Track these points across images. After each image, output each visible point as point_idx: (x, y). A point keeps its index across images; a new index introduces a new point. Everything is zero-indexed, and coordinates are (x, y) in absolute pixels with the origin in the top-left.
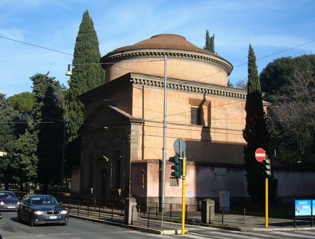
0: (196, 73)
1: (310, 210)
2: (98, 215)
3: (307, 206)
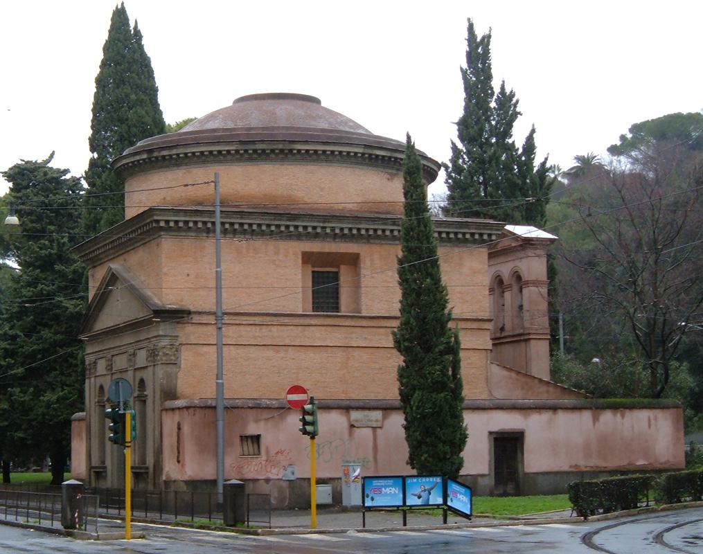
0: (322, 189)
1: (401, 496)
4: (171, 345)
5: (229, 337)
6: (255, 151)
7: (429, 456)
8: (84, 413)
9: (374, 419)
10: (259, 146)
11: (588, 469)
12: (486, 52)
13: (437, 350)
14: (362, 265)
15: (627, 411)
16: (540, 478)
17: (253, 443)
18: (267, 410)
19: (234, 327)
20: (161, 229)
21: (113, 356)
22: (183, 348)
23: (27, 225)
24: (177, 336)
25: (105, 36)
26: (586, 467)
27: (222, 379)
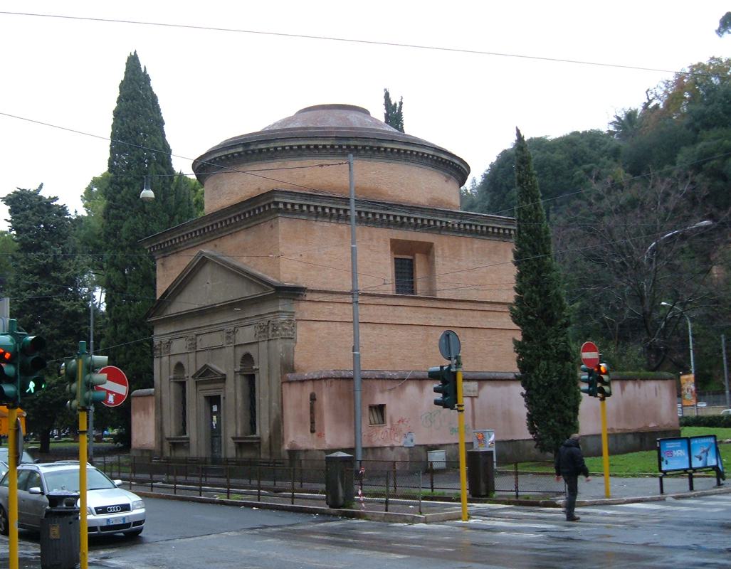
1: (687, 458)
2: (514, 493)
3: (681, 451)
4: (289, 320)
5: (336, 314)
6: (348, 147)
7: (555, 421)
8: (153, 389)
9: (472, 389)
10: (352, 143)
11: (619, 432)
12: (400, 114)
13: (559, 323)
14: (436, 254)
15: (642, 382)
16: (589, 440)
17: (376, 412)
18: (390, 382)
19: (339, 305)
20: (279, 210)
21: (197, 335)
22: (299, 323)
23: (26, 239)
24: (294, 312)
25: (122, 77)
26: (618, 430)
27: (358, 351)
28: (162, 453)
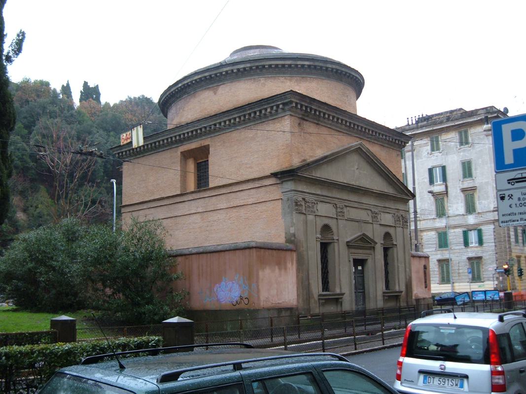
28: (309, 310)
